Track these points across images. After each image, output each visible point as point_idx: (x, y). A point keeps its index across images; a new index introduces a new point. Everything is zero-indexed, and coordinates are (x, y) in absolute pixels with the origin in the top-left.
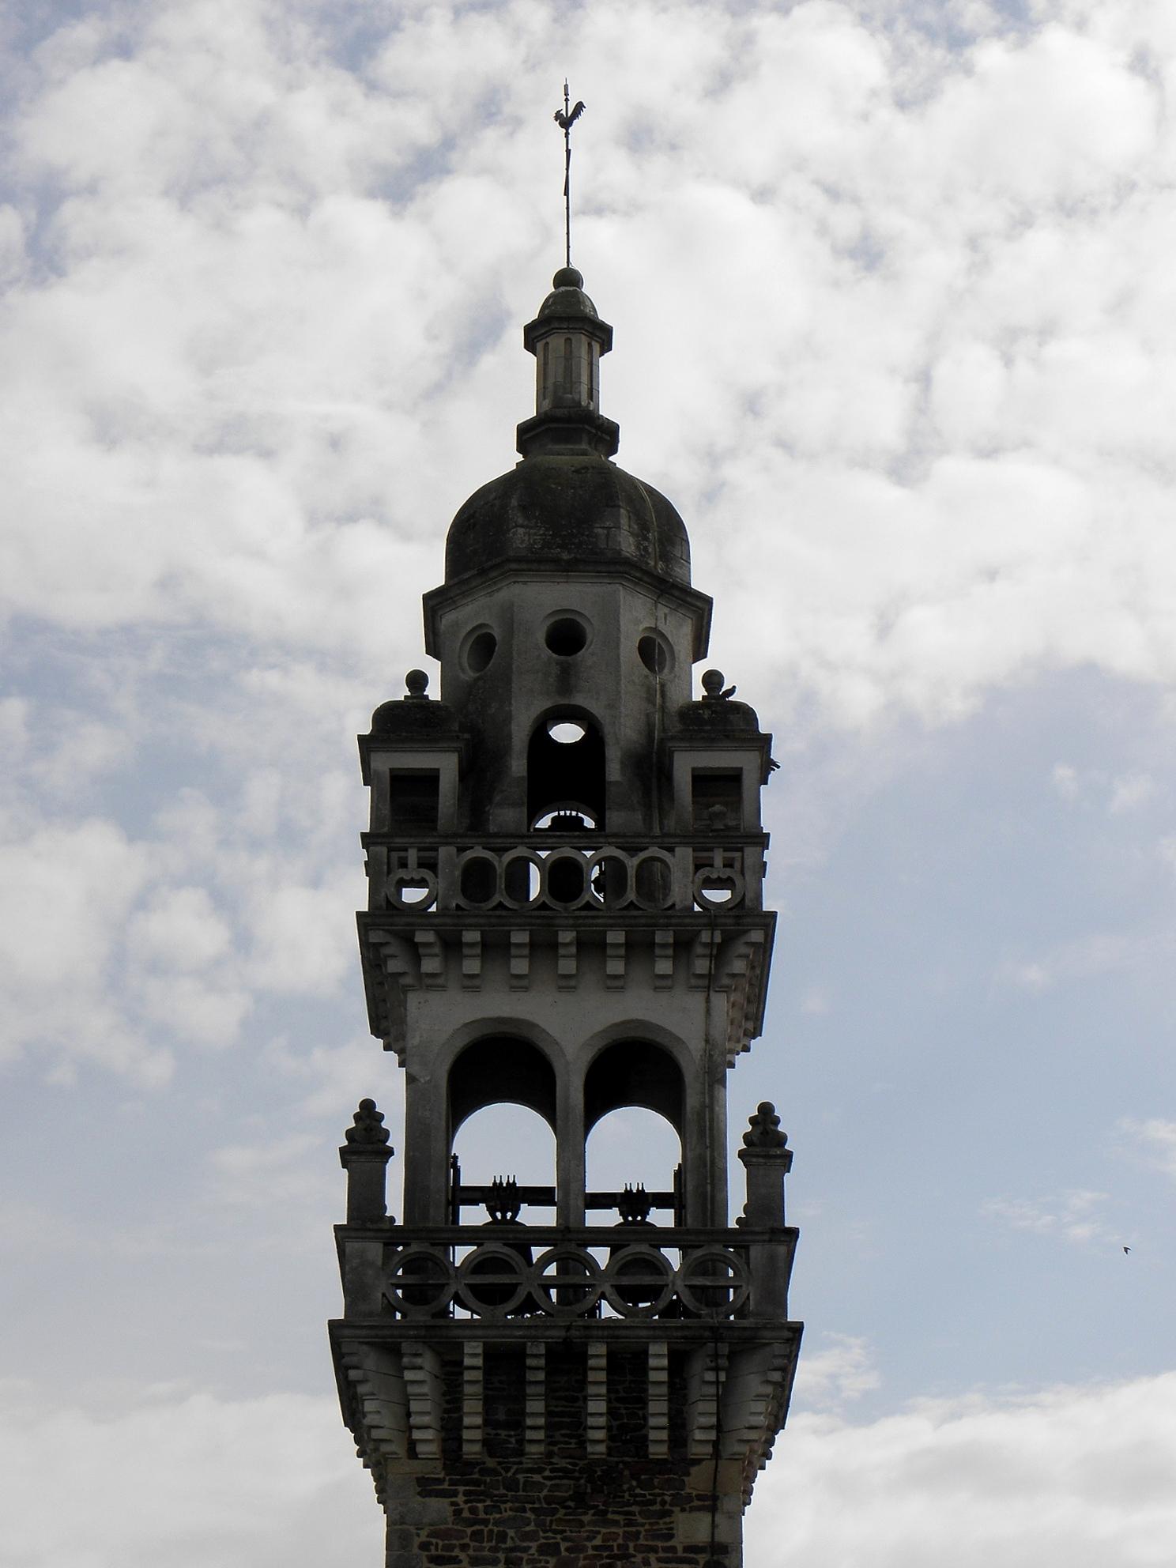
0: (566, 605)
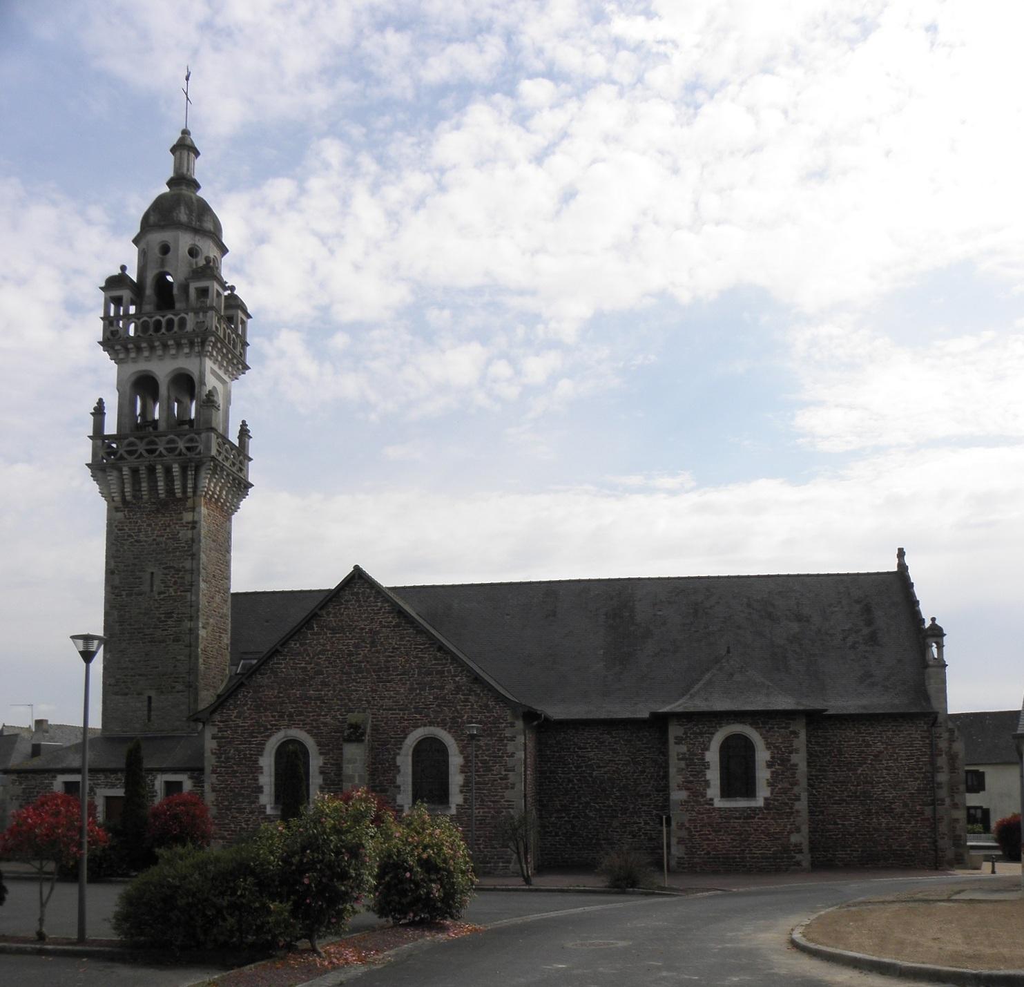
0: (164, 239)
